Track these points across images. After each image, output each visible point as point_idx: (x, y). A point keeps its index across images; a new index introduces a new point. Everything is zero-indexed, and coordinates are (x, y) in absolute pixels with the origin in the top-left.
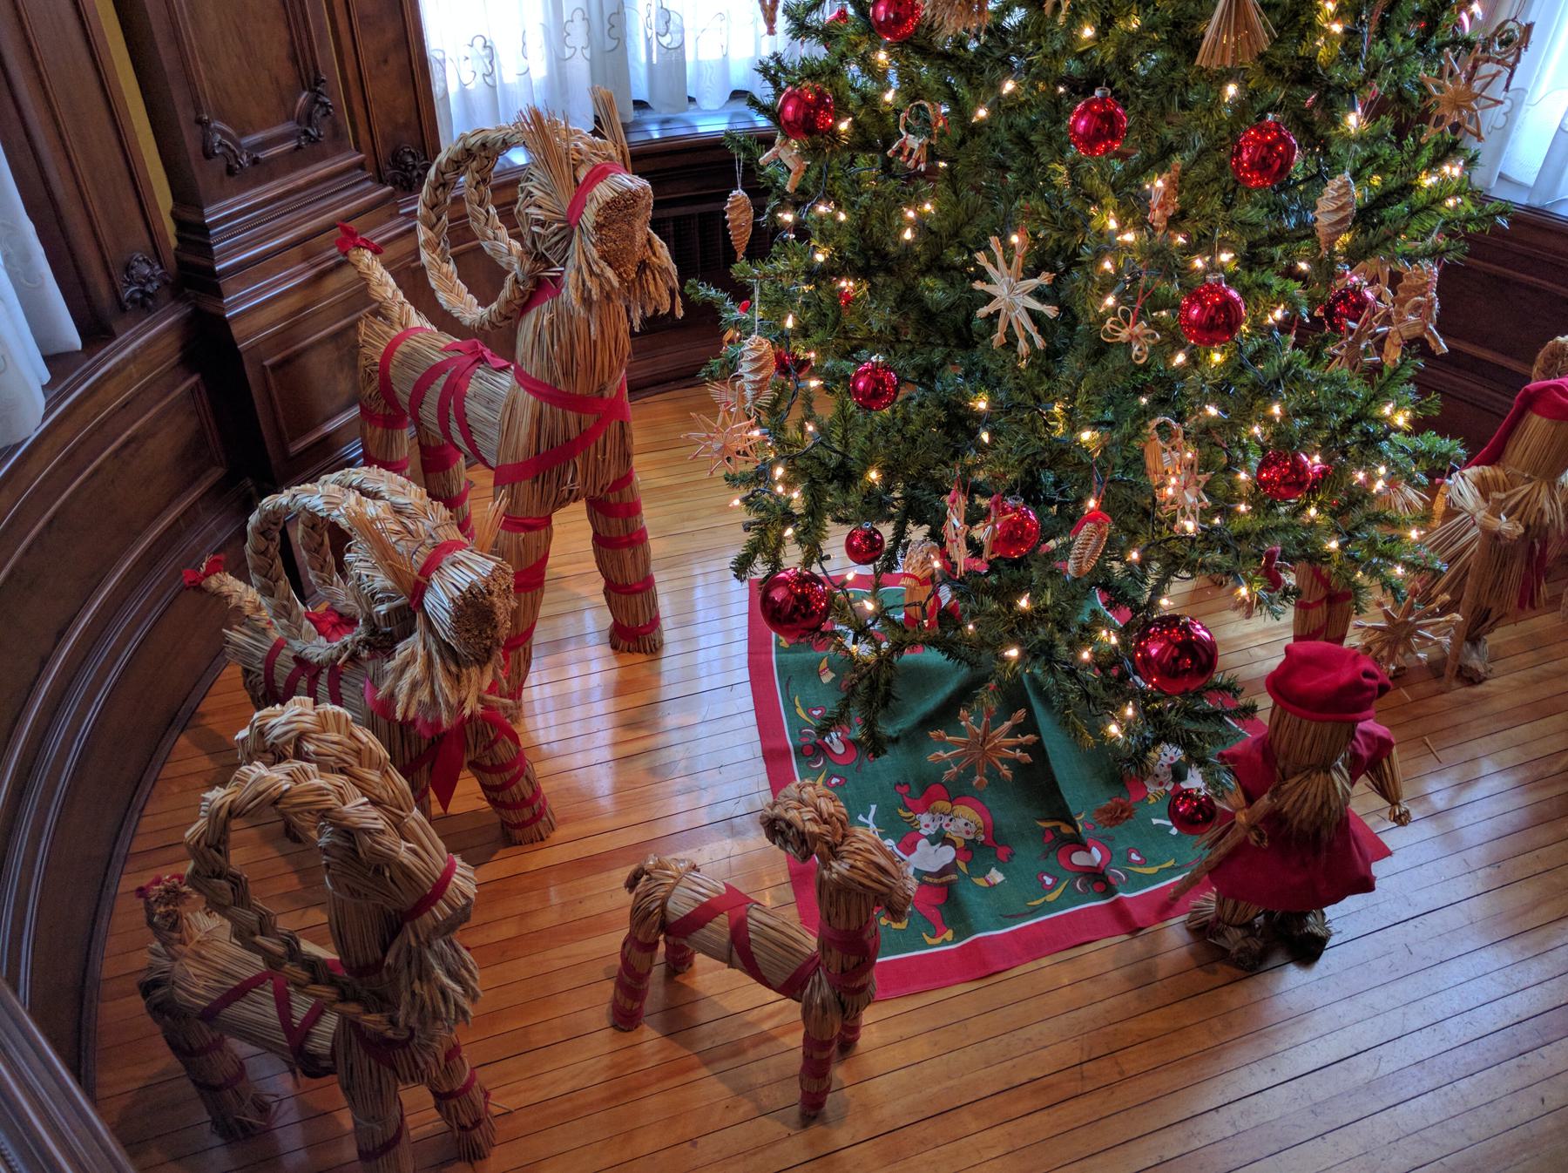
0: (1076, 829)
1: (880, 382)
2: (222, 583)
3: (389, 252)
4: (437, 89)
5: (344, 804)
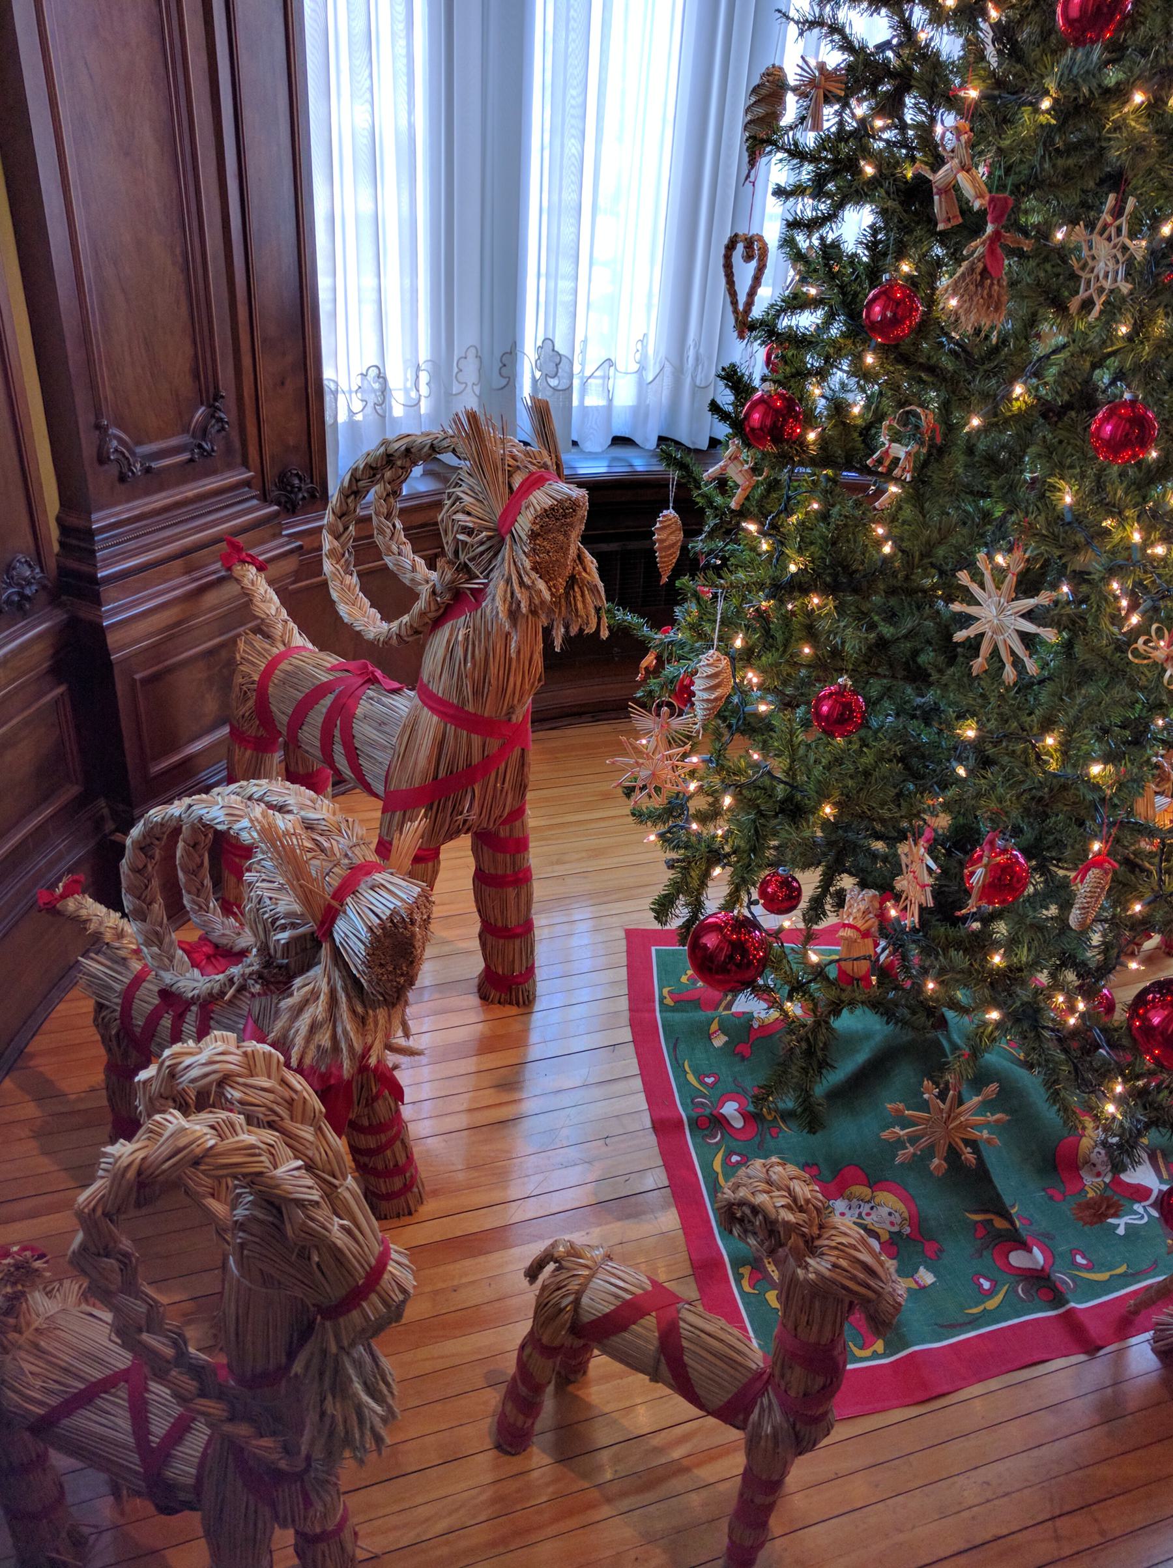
0: (1013, 1223)
1: (847, 706)
2: (80, 906)
3: (273, 569)
4: (328, 419)
5: (275, 1167)
